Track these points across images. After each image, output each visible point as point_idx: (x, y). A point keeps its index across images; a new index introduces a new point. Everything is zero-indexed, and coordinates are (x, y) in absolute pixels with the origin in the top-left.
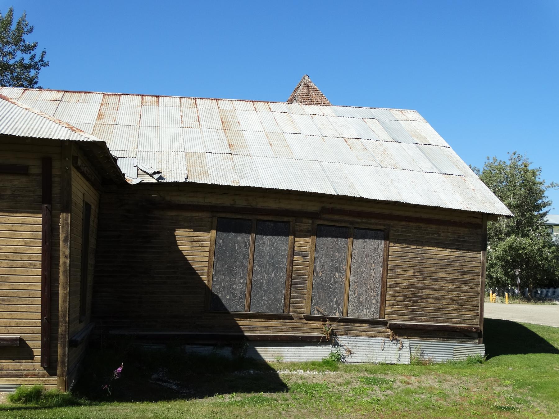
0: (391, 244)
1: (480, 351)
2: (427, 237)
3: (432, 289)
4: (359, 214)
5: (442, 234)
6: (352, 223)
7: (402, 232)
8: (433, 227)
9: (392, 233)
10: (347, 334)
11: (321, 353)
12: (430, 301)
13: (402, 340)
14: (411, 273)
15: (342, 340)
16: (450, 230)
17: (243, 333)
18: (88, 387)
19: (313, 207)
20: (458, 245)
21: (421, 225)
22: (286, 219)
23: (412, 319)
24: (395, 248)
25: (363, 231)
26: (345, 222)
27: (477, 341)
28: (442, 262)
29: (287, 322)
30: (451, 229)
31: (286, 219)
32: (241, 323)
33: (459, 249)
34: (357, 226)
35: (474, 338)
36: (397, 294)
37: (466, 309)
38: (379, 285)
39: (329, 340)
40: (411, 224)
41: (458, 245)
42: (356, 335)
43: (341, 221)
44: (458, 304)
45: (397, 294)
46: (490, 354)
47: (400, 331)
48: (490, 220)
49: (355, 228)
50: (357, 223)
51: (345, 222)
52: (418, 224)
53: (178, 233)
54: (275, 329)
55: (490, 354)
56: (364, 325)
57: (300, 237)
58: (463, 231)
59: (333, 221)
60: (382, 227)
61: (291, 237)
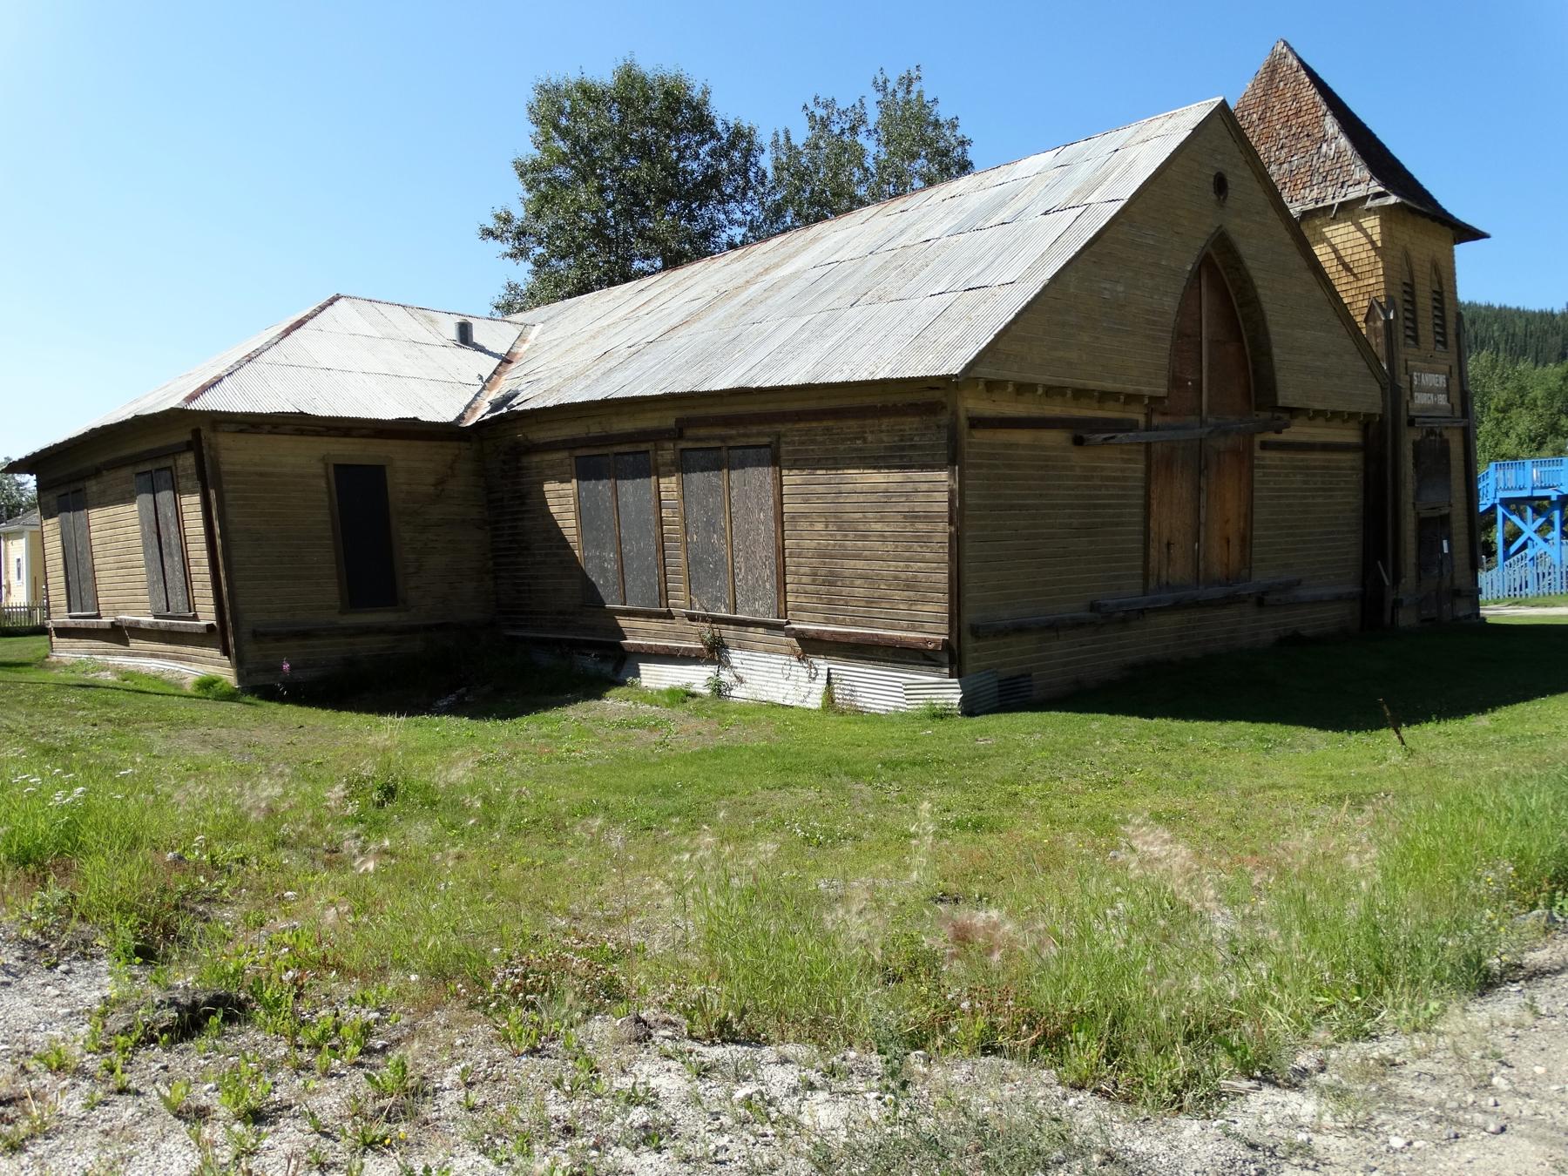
0: (785, 472)
1: (951, 694)
2: (842, 447)
3: (857, 557)
4: (727, 421)
5: (870, 437)
6: (723, 439)
7: (803, 443)
8: (852, 425)
9: (784, 448)
10: (740, 647)
11: (697, 677)
12: (858, 582)
13: (815, 661)
14: (820, 526)
15: (736, 657)
16: (884, 427)
17: (1476, 605)
18: (993, 695)
19: (668, 420)
20: (902, 457)
21: (830, 423)
22: (643, 447)
23: (828, 622)
24: (791, 478)
25: (740, 452)
26: (713, 438)
27: (947, 670)
28: (873, 498)
29: (668, 624)
30: (886, 423)
31: (643, 447)
32: (623, 622)
33: (903, 467)
34: (732, 444)
35: (942, 666)
36: (803, 570)
37: (925, 601)
38: (772, 553)
39: (715, 653)
40: (814, 424)
41: (902, 457)
42: (752, 649)
43: (708, 439)
44: (908, 588)
45: (803, 570)
46: (970, 708)
47: (811, 646)
48: (40, 487)
49: (730, 448)
50: (731, 437)
51: (713, 438)
52: (825, 424)
53: (547, 487)
54: (657, 635)
55: (970, 708)
56: (761, 630)
57: (665, 476)
58: (910, 424)
59: (699, 440)
60: (766, 440)
61: (654, 478)
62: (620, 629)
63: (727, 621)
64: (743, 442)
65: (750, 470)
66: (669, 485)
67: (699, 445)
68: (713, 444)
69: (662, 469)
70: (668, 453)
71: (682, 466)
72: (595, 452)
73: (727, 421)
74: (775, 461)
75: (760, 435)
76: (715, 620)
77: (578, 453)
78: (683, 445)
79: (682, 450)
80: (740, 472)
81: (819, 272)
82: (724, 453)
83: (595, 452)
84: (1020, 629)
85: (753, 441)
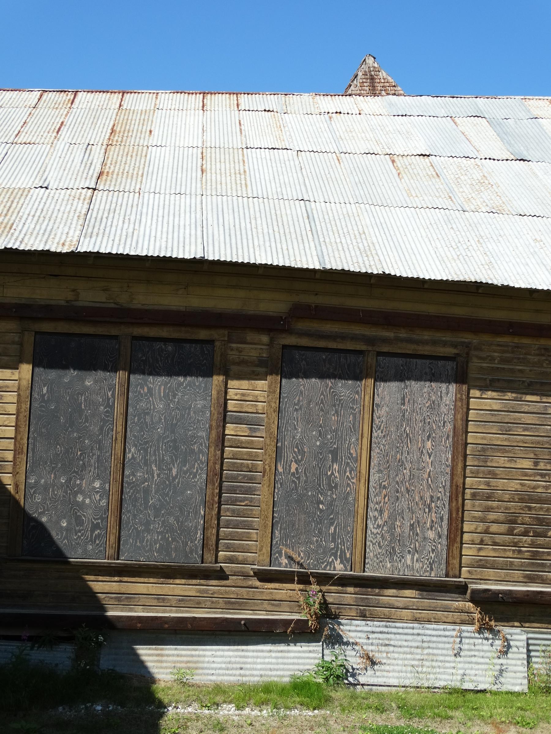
0: (474, 393)
4: (389, 320)
6: (371, 341)
9: (475, 364)
11: (299, 660)
15: (352, 629)
19: (272, 304)
23: (531, 579)
24: (485, 402)
31: (203, 334)
32: (100, 585)
36: (492, 516)
39: (319, 628)
40: (526, 341)
42: (388, 618)
43: (343, 337)
49: (379, 354)
51: (354, 338)
56: (408, 593)
57: (239, 377)
60: (450, 351)
61: (217, 380)
62: (93, 595)
63: (343, 581)
64: (410, 349)
65: (414, 385)
66: (251, 394)
67: (322, 344)
68: (350, 345)
69: (234, 369)
70: (257, 345)
71: (285, 365)
72: (100, 330)
73: (389, 320)
74: (461, 377)
75: (445, 344)
76: (324, 579)
77: (47, 327)
78: (291, 340)
79: (284, 347)
80: (394, 386)
81: (506, 144)
82: (371, 360)
83: (100, 330)
84: (254, 631)
85: (426, 350)
